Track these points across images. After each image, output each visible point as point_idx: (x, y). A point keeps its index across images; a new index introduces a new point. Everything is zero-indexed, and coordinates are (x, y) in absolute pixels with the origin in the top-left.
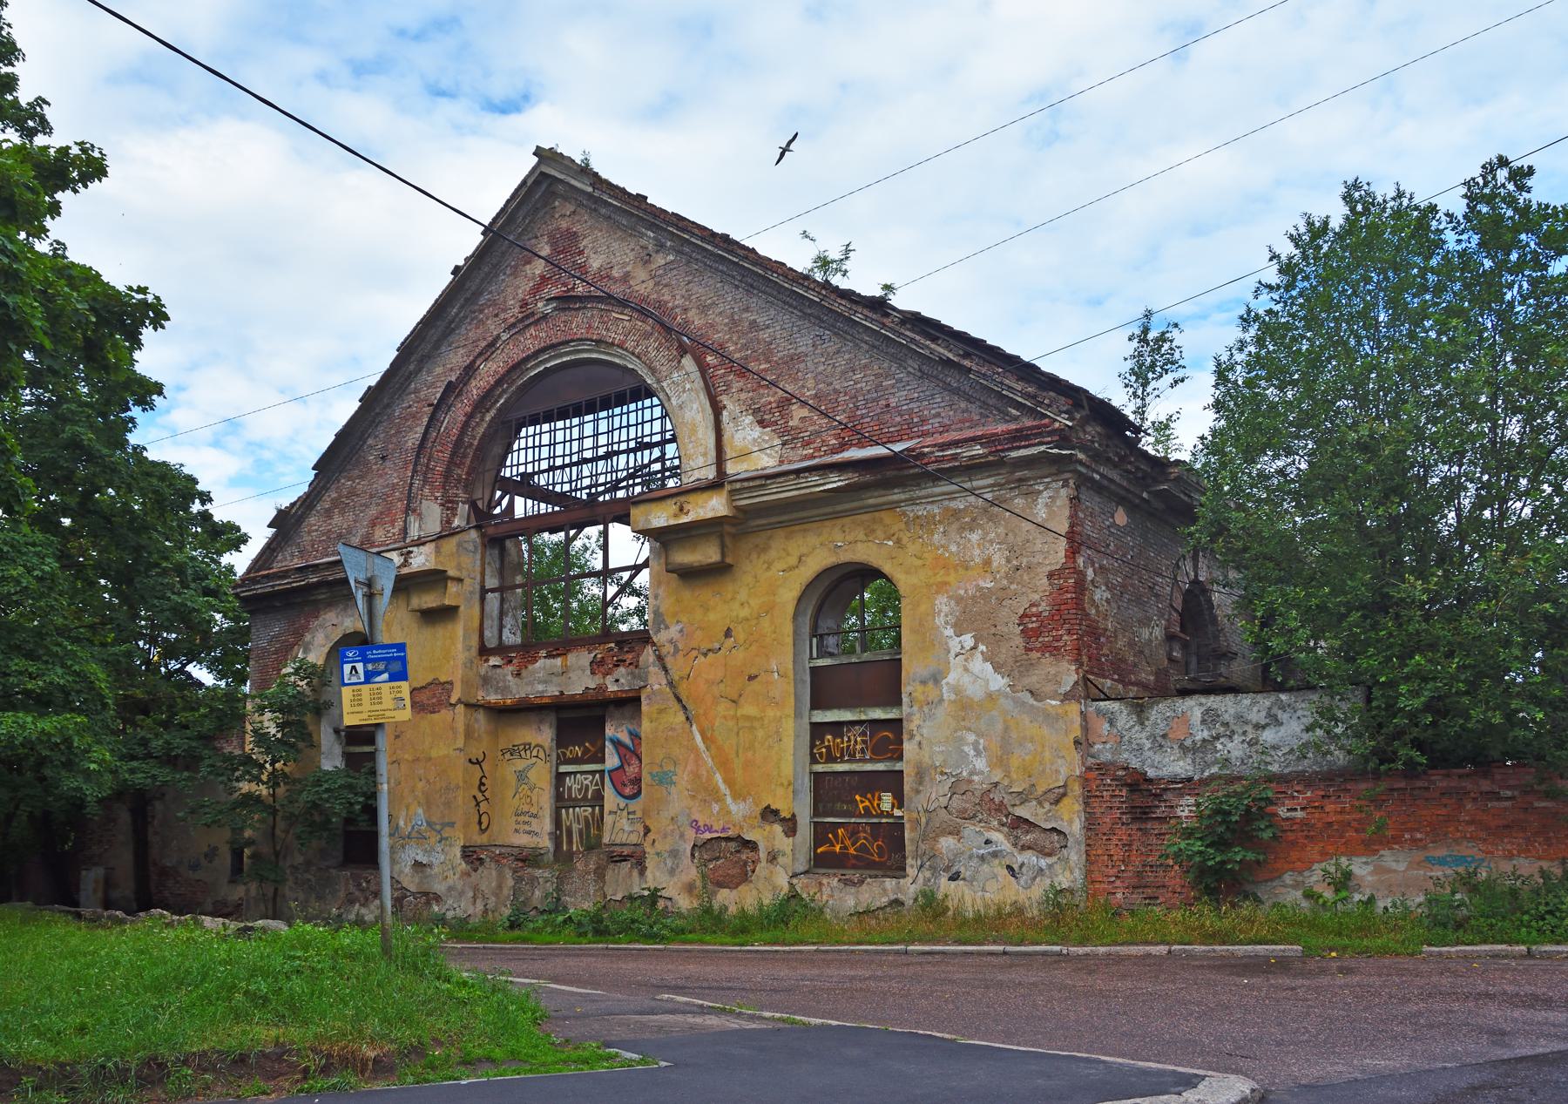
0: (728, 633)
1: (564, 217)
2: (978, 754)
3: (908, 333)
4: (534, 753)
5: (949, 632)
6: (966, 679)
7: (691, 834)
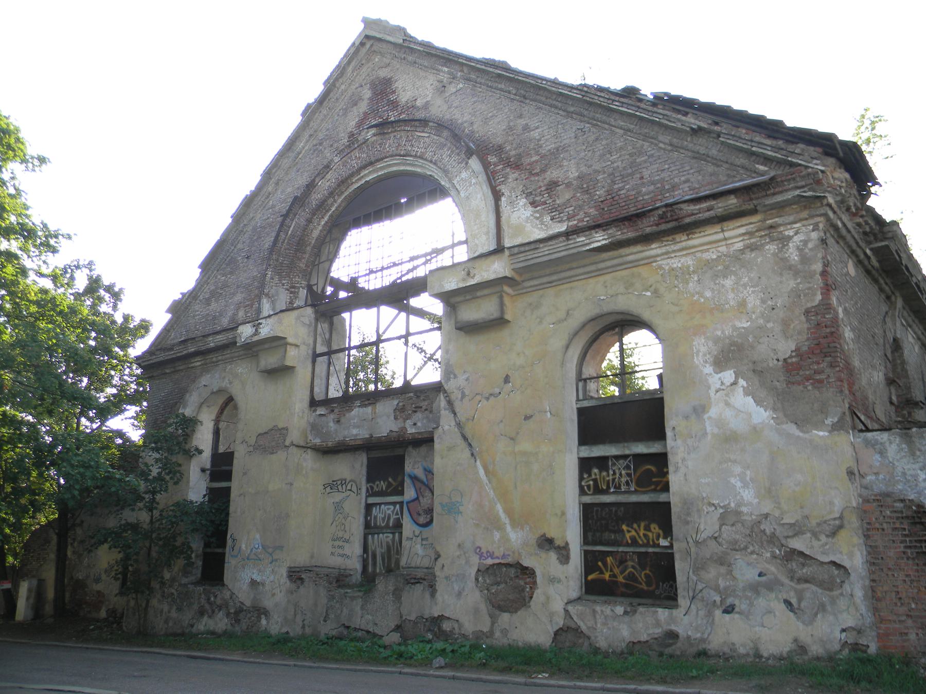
0: (507, 380)
2: (745, 485)
3: (661, 111)
4: (349, 487)
5: (709, 369)
6: (728, 414)
7: (475, 560)
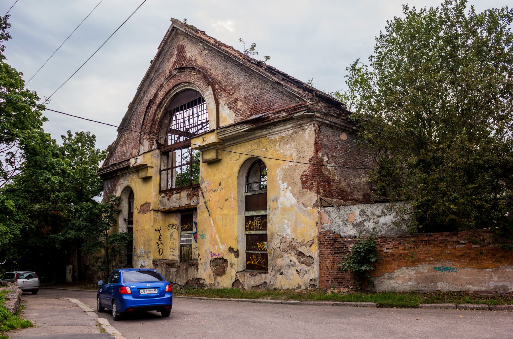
0: (220, 184)
1: (182, 41)
5: (280, 182)
